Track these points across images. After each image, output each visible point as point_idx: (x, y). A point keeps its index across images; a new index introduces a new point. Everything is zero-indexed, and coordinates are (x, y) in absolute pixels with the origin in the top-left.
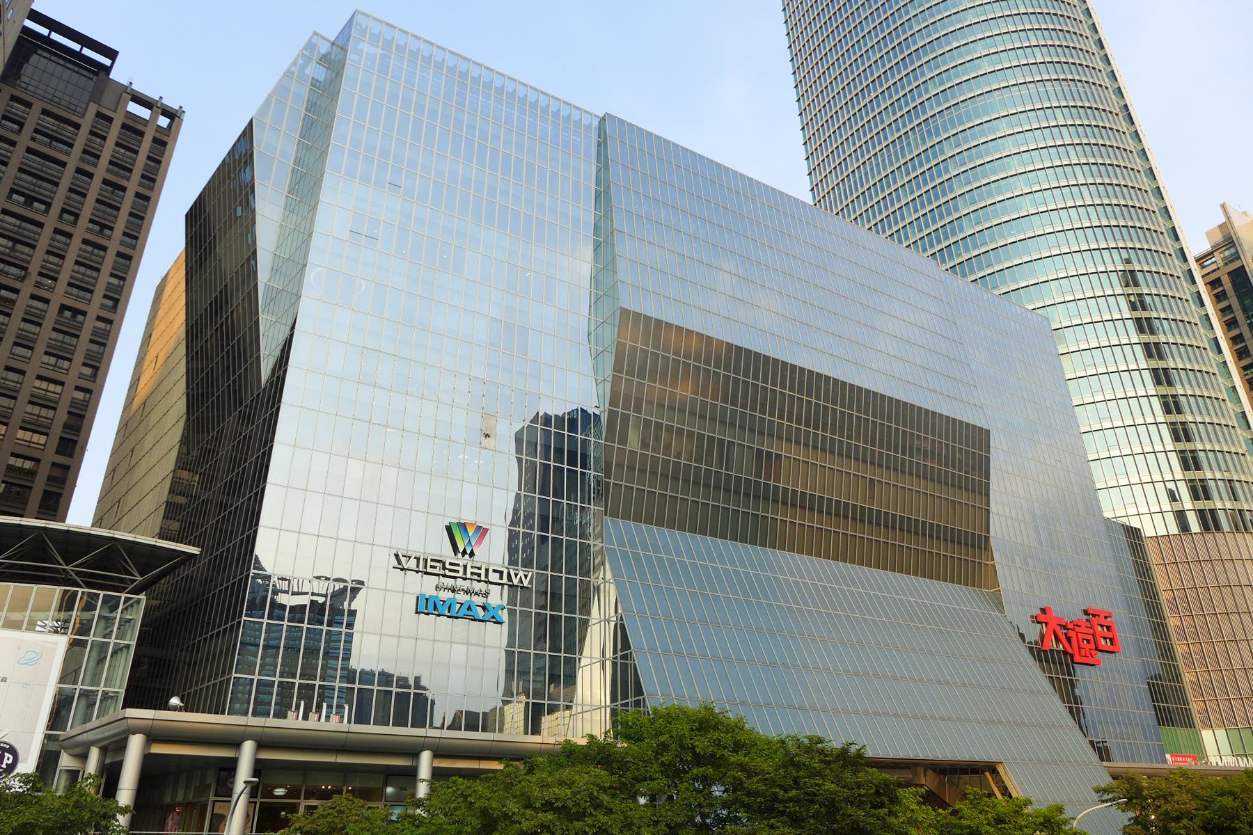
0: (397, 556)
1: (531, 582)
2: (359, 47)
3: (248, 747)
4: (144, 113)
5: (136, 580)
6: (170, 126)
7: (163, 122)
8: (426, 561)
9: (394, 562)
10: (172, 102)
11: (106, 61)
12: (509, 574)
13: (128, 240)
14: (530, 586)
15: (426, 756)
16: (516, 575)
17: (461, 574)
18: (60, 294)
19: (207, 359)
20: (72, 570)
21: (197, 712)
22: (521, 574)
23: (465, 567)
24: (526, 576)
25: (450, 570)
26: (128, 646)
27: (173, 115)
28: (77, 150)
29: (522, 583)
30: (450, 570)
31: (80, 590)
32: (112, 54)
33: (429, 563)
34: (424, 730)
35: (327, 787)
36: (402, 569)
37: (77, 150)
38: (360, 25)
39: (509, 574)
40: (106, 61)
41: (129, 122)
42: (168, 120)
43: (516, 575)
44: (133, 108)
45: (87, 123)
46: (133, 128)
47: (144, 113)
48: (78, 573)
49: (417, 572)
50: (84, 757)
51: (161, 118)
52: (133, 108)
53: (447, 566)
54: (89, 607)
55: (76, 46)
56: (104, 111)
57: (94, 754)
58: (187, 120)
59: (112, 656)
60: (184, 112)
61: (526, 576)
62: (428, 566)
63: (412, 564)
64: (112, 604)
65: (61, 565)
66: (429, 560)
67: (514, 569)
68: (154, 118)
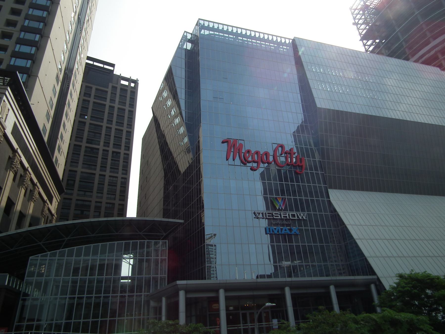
0: (254, 213)
1: (306, 217)
2: (201, 33)
3: (222, 292)
4: (126, 83)
5: (163, 235)
6: (135, 86)
7: (133, 85)
8: (266, 214)
9: (254, 216)
10: (134, 78)
11: (112, 68)
12: (297, 215)
13: (129, 126)
14: (306, 219)
15: (222, 292)
16: (300, 215)
17: (279, 217)
18: (111, 149)
19: (165, 157)
20: (142, 234)
21: (191, 280)
22: (302, 214)
23: (280, 215)
24: (304, 215)
25: (276, 216)
26: (165, 259)
27: (136, 82)
28: (108, 100)
29: (299, 218)
30: (276, 216)
31: (146, 241)
32: (113, 65)
33: (267, 215)
34: (285, 278)
35: (246, 305)
36: (257, 218)
37: (108, 100)
38: (201, 24)
39: (297, 215)
40: (112, 68)
41: (123, 87)
42: (134, 84)
43: (300, 215)
44: (123, 82)
45: (109, 90)
46: (124, 89)
47: (126, 83)
48: (144, 235)
49: (263, 218)
50: (160, 301)
51: (132, 84)
52: (123, 82)
53: (274, 215)
54: (148, 247)
55: (101, 65)
56: (114, 85)
57: (164, 299)
58: (140, 82)
59: (161, 263)
60: (138, 80)
61: (304, 215)
62: (267, 216)
63: (261, 216)
64: (156, 244)
65: (137, 232)
66: (267, 213)
67: (299, 213)
68: (130, 84)
